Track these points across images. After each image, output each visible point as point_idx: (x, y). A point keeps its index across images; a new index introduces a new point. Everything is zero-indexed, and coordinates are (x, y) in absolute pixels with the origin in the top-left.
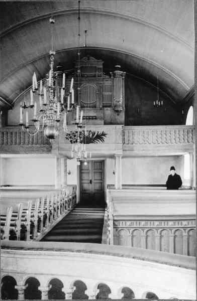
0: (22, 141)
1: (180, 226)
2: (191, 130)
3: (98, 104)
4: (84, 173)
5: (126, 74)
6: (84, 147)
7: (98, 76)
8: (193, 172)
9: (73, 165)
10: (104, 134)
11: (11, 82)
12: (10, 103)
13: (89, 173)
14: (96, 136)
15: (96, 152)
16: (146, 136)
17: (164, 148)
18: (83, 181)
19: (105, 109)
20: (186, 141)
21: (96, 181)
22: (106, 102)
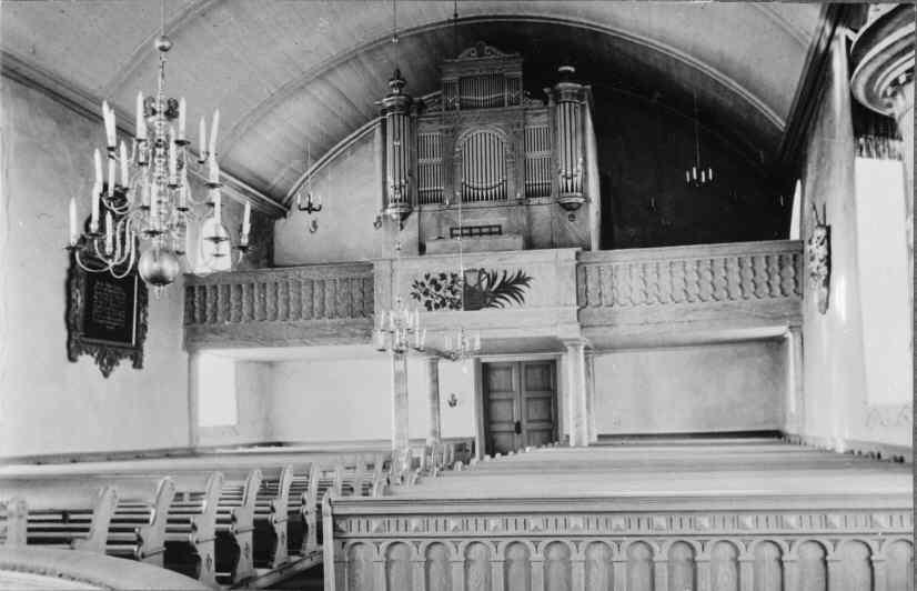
0: (292, 309)
1: (521, 531)
2: (791, 257)
3: (511, 187)
4: (499, 400)
5: (593, 89)
6: (463, 316)
7: (511, 104)
8: (801, 389)
9: (461, 379)
10: (521, 279)
11: (268, 138)
12: (280, 201)
13: (511, 400)
14: (500, 287)
15: (490, 334)
16: (652, 278)
17: (709, 314)
18: (496, 427)
19: (534, 201)
20: (777, 291)
21: (531, 426)
22: (537, 180)
